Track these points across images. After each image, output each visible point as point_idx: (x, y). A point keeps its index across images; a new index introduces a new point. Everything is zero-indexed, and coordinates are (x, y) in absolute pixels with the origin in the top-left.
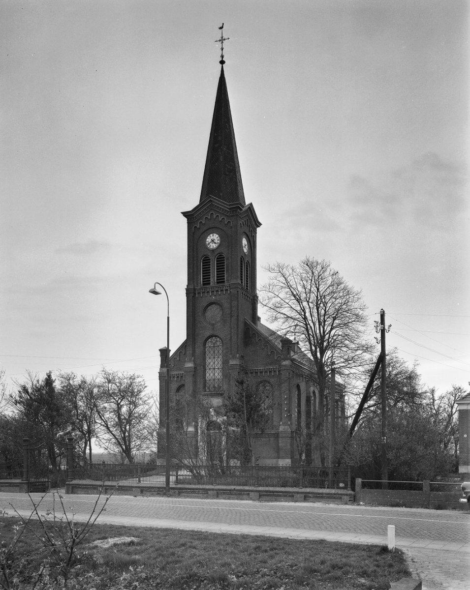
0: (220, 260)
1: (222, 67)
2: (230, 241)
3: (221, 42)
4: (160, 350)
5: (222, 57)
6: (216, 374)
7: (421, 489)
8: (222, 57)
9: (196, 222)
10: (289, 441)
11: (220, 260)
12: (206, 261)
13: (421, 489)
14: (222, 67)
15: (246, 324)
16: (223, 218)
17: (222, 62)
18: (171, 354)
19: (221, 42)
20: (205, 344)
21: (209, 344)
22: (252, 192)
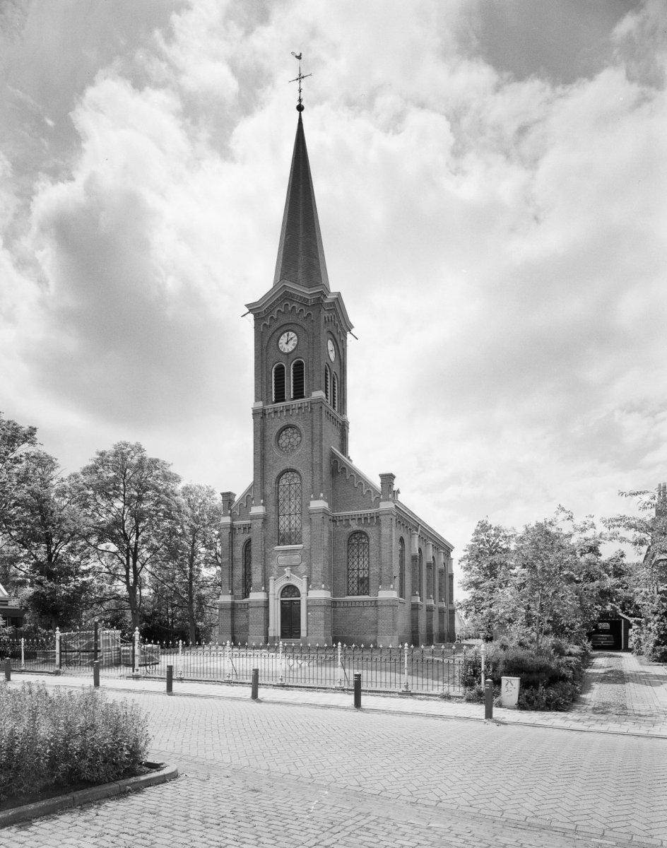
0: (299, 368)
1: (300, 114)
2: (310, 341)
3: (298, 81)
4: (252, 308)
5: (300, 100)
6: (293, 522)
7: (359, 676)
8: (300, 100)
9: (268, 318)
10: (230, 612)
11: (299, 368)
12: (280, 372)
13: (359, 676)
14: (300, 114)
15: (333, 455)
16: (302, 310)
17: (300, 108)
18: (236, 499)
19: (298, 81)
20: (280, 477)
21: (283, 481)
22: (340, 276)
